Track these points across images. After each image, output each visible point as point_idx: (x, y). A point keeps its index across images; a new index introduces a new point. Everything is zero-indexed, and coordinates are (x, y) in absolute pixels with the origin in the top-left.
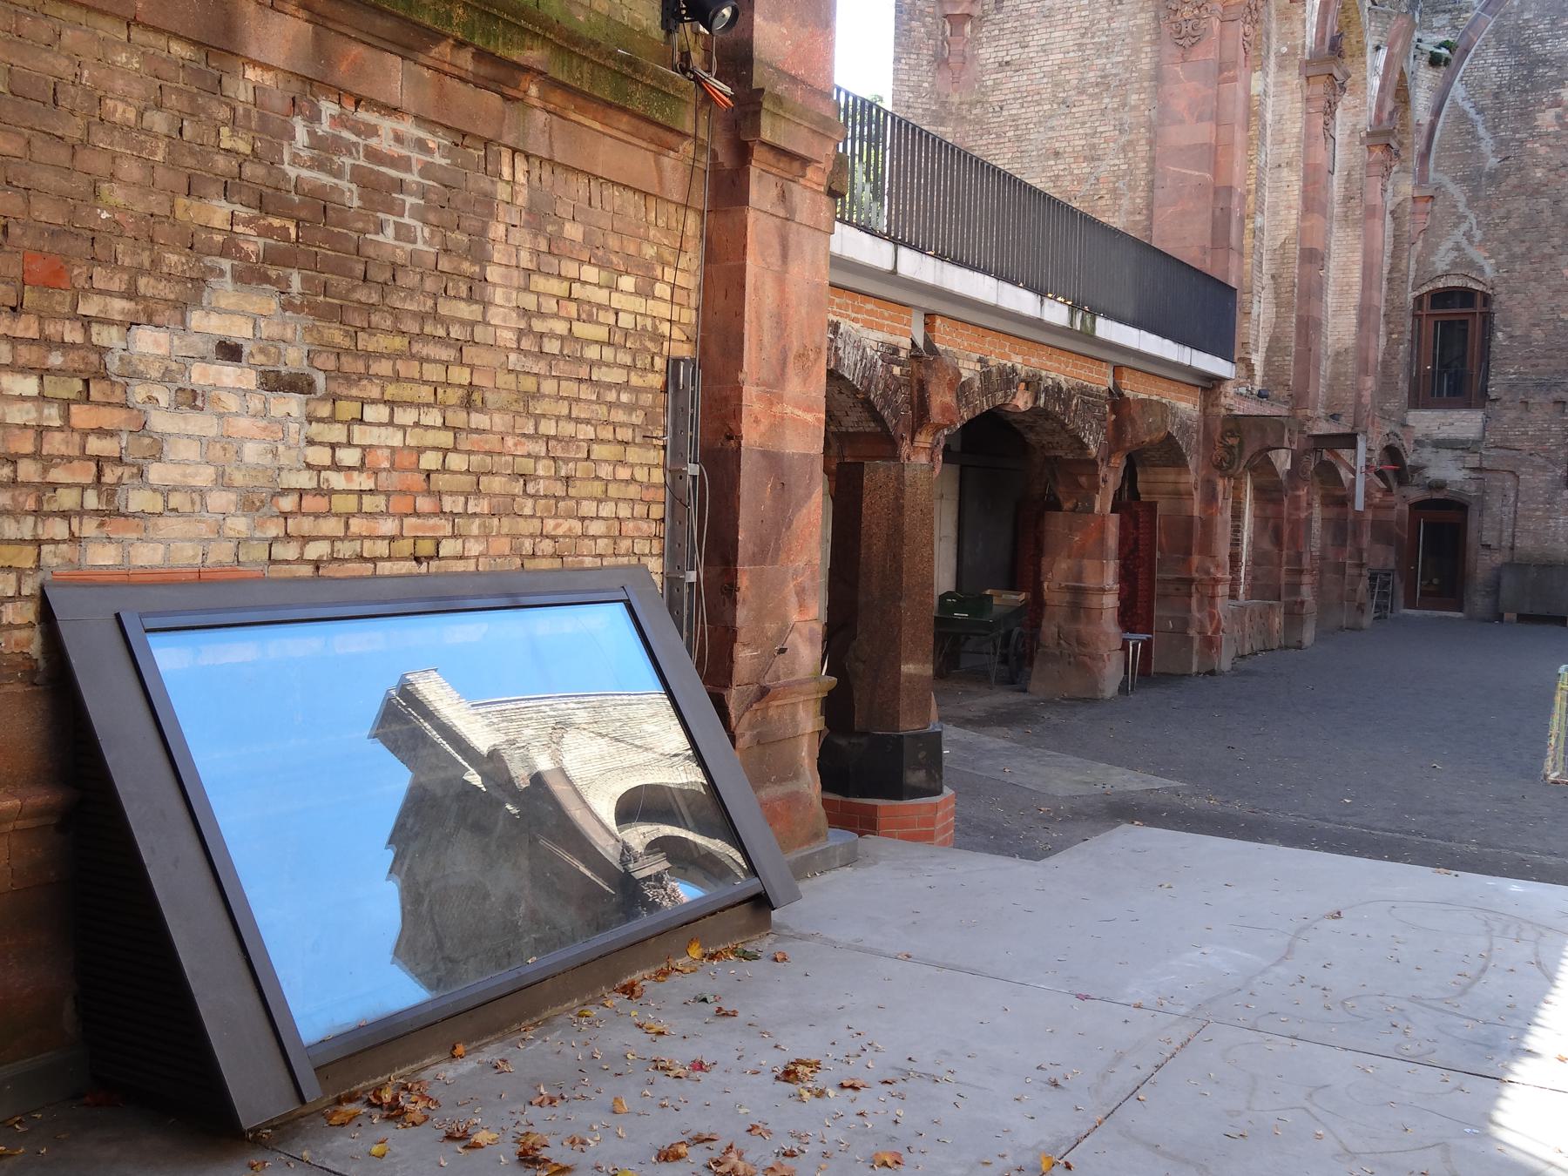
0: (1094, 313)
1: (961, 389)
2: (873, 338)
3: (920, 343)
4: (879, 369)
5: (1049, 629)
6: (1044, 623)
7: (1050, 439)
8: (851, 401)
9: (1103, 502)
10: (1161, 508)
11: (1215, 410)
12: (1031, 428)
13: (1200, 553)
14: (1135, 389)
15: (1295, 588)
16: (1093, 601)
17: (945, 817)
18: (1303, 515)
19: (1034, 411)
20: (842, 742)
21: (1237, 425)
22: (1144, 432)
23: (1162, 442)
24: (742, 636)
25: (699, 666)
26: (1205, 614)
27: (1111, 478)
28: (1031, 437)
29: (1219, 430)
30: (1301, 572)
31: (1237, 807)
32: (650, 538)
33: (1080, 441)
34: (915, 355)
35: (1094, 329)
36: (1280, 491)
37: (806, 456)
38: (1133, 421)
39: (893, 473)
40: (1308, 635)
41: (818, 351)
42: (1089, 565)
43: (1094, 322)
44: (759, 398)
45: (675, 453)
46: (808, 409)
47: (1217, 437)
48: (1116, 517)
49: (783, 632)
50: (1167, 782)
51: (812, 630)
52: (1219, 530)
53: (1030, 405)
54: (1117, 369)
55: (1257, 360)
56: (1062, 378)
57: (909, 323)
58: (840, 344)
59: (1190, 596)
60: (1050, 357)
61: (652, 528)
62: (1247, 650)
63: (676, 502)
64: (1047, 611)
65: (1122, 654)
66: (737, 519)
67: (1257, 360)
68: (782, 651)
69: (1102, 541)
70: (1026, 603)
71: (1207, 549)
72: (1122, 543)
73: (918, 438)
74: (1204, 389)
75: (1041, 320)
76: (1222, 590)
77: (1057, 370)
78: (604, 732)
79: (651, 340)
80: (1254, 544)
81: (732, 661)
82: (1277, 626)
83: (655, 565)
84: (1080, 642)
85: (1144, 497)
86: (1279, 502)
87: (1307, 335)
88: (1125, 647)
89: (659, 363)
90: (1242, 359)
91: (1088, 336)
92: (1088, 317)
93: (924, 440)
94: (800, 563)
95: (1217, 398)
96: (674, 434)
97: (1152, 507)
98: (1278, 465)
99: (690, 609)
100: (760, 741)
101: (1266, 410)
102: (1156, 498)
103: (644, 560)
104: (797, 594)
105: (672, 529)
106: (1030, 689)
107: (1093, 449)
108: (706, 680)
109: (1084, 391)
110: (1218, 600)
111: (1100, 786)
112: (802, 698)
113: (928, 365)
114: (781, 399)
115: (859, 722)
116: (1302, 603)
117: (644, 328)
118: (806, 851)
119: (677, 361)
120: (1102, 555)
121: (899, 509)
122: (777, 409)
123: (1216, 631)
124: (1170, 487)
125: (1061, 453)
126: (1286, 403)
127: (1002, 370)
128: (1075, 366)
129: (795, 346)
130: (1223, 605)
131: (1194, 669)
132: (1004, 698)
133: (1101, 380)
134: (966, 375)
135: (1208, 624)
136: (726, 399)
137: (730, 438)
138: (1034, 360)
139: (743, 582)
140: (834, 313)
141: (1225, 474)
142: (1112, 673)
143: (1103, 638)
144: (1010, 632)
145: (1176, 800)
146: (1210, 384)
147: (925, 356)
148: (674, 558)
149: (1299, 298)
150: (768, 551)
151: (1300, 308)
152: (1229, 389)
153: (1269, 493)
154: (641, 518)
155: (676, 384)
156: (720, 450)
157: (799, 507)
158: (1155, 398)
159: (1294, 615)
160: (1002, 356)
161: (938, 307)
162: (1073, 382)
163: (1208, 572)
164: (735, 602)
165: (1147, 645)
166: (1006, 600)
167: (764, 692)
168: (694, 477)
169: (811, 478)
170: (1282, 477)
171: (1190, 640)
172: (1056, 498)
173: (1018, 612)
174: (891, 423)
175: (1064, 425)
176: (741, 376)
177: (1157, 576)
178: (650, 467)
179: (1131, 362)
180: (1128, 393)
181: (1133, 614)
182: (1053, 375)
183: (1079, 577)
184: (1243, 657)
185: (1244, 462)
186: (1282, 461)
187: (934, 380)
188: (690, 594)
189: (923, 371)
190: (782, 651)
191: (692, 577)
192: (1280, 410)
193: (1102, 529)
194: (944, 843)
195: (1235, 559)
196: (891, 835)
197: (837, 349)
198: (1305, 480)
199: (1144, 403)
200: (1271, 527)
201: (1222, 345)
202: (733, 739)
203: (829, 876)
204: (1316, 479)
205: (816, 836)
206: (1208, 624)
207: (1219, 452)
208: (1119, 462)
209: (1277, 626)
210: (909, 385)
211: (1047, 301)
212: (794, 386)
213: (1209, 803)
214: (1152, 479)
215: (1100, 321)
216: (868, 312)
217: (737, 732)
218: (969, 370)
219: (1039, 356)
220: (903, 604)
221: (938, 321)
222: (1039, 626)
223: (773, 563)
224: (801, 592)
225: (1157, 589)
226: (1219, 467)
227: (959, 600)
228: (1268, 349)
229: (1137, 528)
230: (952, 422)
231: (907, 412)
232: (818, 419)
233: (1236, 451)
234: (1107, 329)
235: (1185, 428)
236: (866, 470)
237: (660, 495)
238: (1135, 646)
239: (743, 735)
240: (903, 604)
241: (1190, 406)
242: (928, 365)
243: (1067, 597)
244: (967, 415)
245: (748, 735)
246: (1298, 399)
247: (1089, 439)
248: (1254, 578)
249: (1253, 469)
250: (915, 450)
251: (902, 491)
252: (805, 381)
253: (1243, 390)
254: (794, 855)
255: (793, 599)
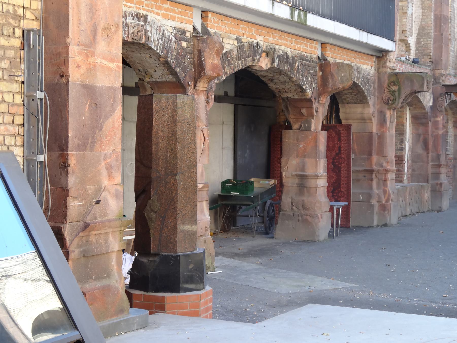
0: (306, 11)
1: (226, 58)
2: (169, 25)
3: (199, 28)
4: (174, 44)
5: (286, 200)
6: (284, 197)
7: (283, 86)
8: (157, 62)
9: (316, 124)
10: (354, 129)
11: (384, 70)
12: (272, 80)
13: (378, 154)
14: (333, 56)
15: (437, 175)
16: (311, 183)
17: (206, 303)
18: (441, 132)
19: (272, 69)
20: (144, 260)
21: (396, 78)
22: (339, 82)
23: (351, 88)
24: (72, 193)
25: (46, 213)
26: (381, 190)
27: (321, 110)
28: (272, 86)
29: (387, 82)
30: (439, 166)
31: (384, 297)
32: (14, 135)
33: (301, 87)
34: (196, 35)
35: (306, 20)
36: (426, 118)
37: (110, 88)
38: (332, 75)
39: (171, 101)
40: (445, 203)
41: (117, 26)
42: (309, 162)
43: (306, 16)
44: (80, 53)
45: (29, 84)
46: (112, 60)
47: (386, 85)
48: (324, 133)
49: (99, 191)
50: (347, 284)
51: (116, 190)
52: (388, 140)
53: (269, 66)
54: (323, 45)
55: (412, 41)
56: (288, 50)
57: (191, 16)
58: (148, 28)
59: (372, 180)
60: (280, 37)
61: (16, 130)
62: (408, 212)
63: (31, 114)
64: (285, 190)
65: (330, 214)
66: (67, 124)
67: (412, 41)
68: (98, 202)
69: (316, 146)
70: (274, 187)
71: (381, 152)
72: (329, 148)
73: (198, 84)
74: (378, 57)
75: (272, 15)
76: (391, 176)
77: (286, 45)
78: (28, 277)
79: (13, 18)
80: (412, 150)
81: (66, 207)
82: (426, 198)
83: (18, 152)
84: (304, 208)
85: (344, 122)
86: (425, 125)
87: (440, 26)
88: (331, 208)
89: (18, 32)
90: (402, 41)
91: (303, 25)
92: (302, 14)
93: (202, 85)
94: (109, 150)
95: (385, 62)
96: (29, 74)
97: (348, 127)
98: (425, 103)
99: (40, 177)
100: (85, 255)
101: (416, 69)
102: (350, 122)
103: (11, 148)
104: (107, 169)
105: (29, 130)
106: (276, 236)
107: (309, 93)
108: (50, 219)
109: (302, 58)
110: (389, 183)
111: (307, 288)
112: (111, 230)
113: (203, 41)
114: (93, 54)
115: (153, 249)
116: (441, 184)
117: (8, 12)
118: (115, 320)
119: (29, 31)
120: (316, 155)
121: (175, 122)
122: (91, 60)
123: (387, 201)
124: (359, 116)
125: (289, 95)
126: (429, 66)
127: (250, 45)
128: (296, 43)
129: (102, 23)
130: (392, 186)
131: (375, 223)
132: (261, 241)
133: (314, 51)
134: (227, 47)
135: (382, 196)
136: (59, 54)
137: (62, 76)
138: (271, 39)
139: (72, 161)
140: (144, 10)
141: (392, 108)
142: (324, 224)
143: (317, 205)
144: (265, 203)
145: (351, 294)
146: (381, 55)
147: (202, 36)
148: (30, 147)
149: (436, 4)
150: (86, 144)
151: (436, 10)
152: (393, 57)
153: (420, 120)
154: (9, 124)
155: (29, 45)
156: (57, 84)
157: (107, 117)
158: (347, 62)
159: (437, 192)
160: (251, 36)
161: (326, 40)
162: (295, 52)
163: (382, 166)
164: (67, 173)
165: (346, 210)
166: (261, 184)
167: (86, 226)
168: (41, 100)
169: (114, 101)
170: (428, 110)
171: (372, 206)
172: (289, 123)
173: (269, 191)
174: (182, 76)
175: (290, 78)
176: (68, 40)
177: (352, 168)
178: (14, 93)
179: (331, 41)
180: (330, 60)
181: (338, 189)
182: (283, 48)
183: (303, 169)
184: (406, 216)
185: (401, 100)
186: (427, 100)
187: (207, 50)
188: (41, 168)
189: (201, 45)
190: (98, 202)
191: (41, 158)
192: (426, 70)
193: (316, 140)
194: (207, 317)
195: (400, 160)
196: (174, 313)
197: (146, 31)
198: (441, 111)
199: (339, 65)
200: (423, 140)
201: (386, 29)
202: (67, 254)
203: (129, 335)
204: (450, 112)
205: (122, 311)
206: (382, 196)
207: (387, 95)
208: (326, 100)
209: (426, 198)
210: (192, 53)
211: (276, 3)
212: (102, 46)
213: (371, 295)
214: (348, 111)
215: (310, 16)
216: (166, 10)
217: (70, 249)
218: (229, 45)
219: (274, 37)
220: (177, 178)
221: (210, 15)
222: (280, 197)
223: (91, 150)
224: (109, 168)
225: (353, 176)
226: (387, 103)
227: (234, 184)
228: (418, 34)
229: (340, 140)
230: (219, 75)
231: (191, 70)
232: (118, 67)
233: (397, 94)
234: (314, 21)
235: (366, 80)
236: (155, 99)
237: (21, 110)
238: (338, 210)
239: (73, 251)
240: (177, 178)
241: (369, 67)
242: (203, 41)
243: (297, 181)
244: (229, 71)
245: (77, 251)
246: (436, 63)
247: (306, 86)
248: (413, 170)
249: (410, 105)
250: (197, 92)
251: (176, 111)
252: (109, 44)
253: (403, 59)
254: (106, 323)
255: (104, 173)
